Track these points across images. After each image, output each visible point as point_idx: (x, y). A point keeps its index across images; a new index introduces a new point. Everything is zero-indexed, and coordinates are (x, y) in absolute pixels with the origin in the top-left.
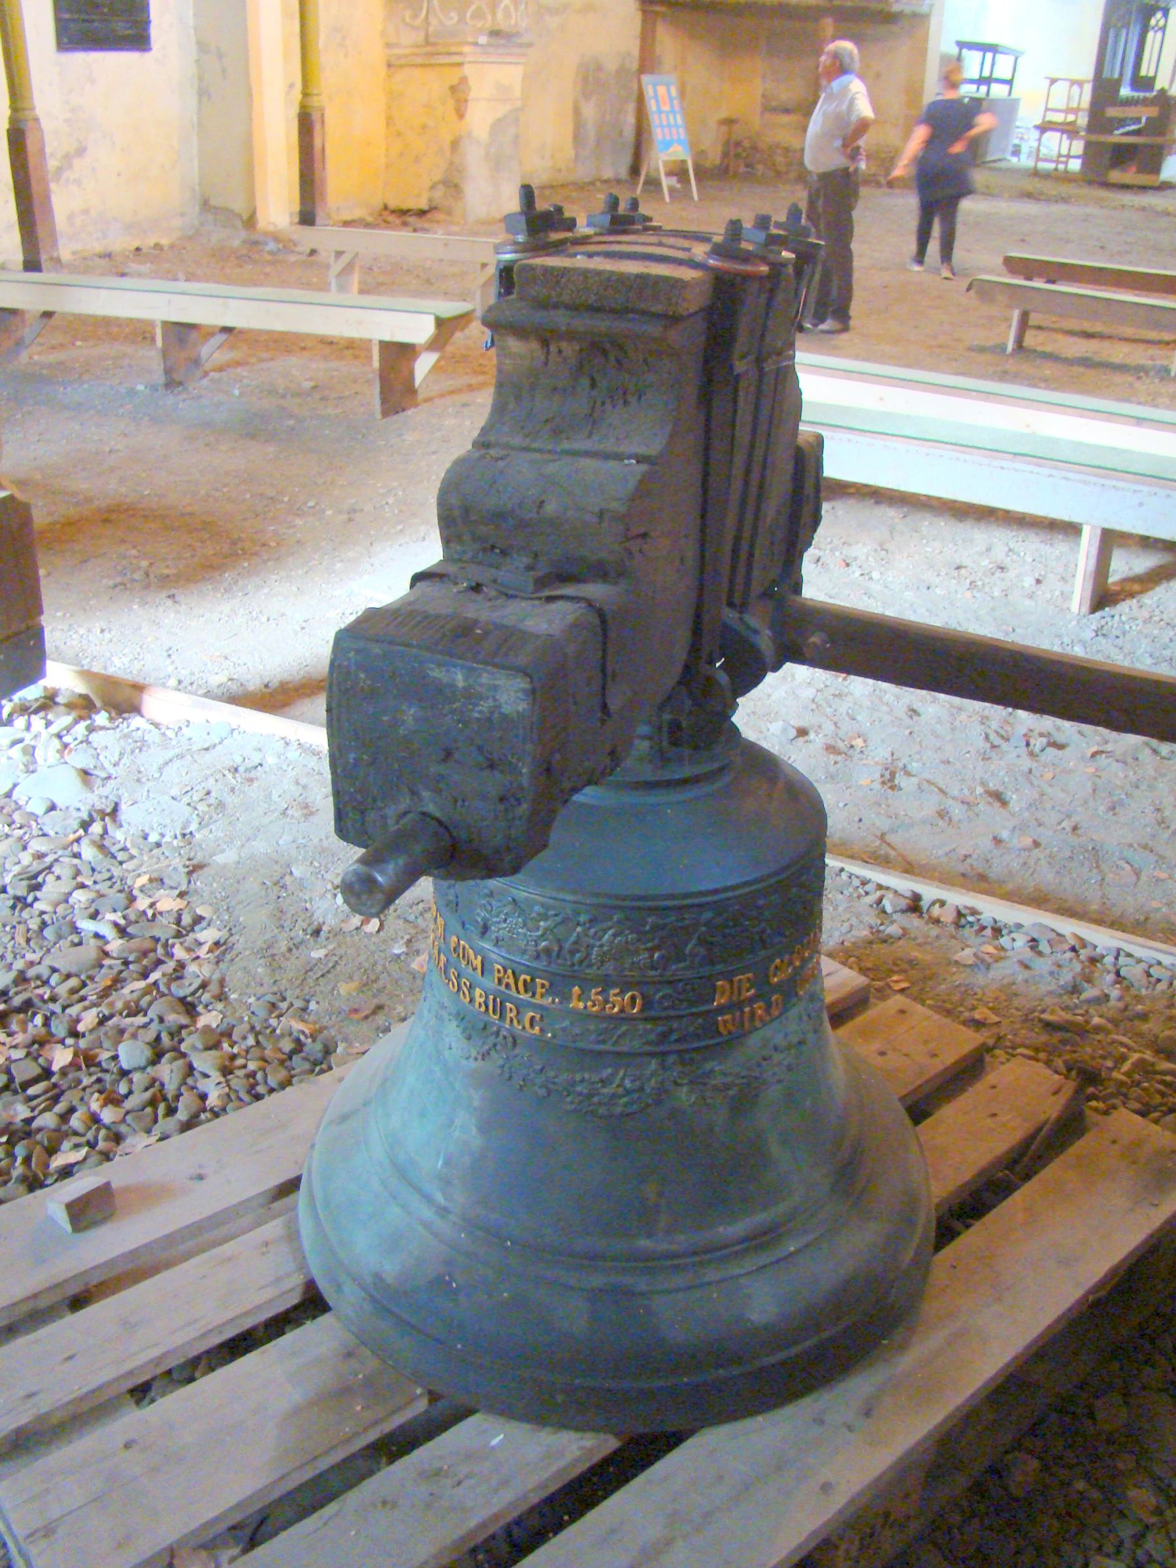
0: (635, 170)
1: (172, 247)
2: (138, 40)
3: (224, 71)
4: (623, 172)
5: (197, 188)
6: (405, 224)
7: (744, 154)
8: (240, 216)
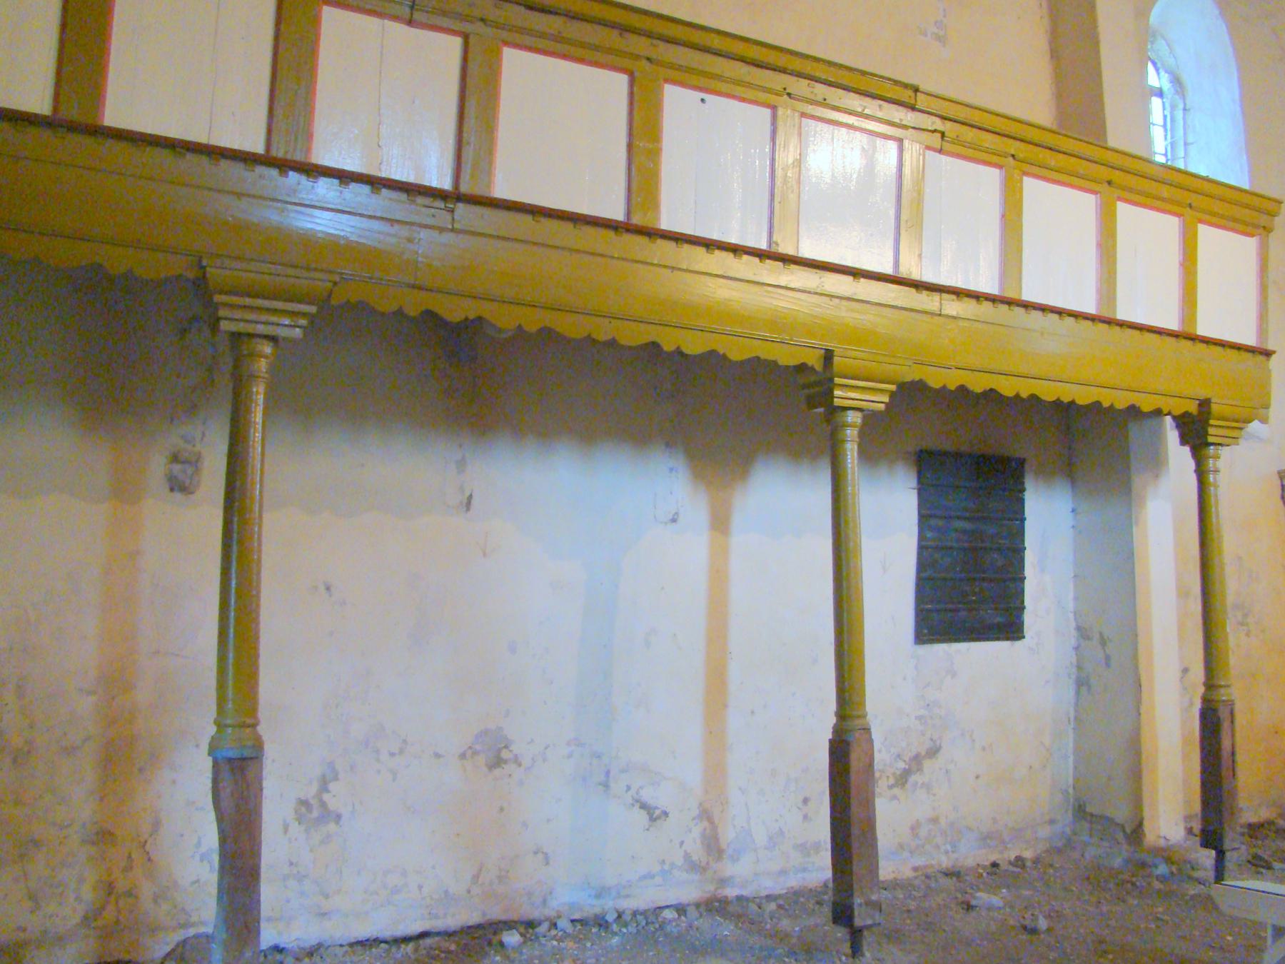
1: (1036, 861)
2: (1011, 628)
3: (1108, 658)
5: (1071, 790)
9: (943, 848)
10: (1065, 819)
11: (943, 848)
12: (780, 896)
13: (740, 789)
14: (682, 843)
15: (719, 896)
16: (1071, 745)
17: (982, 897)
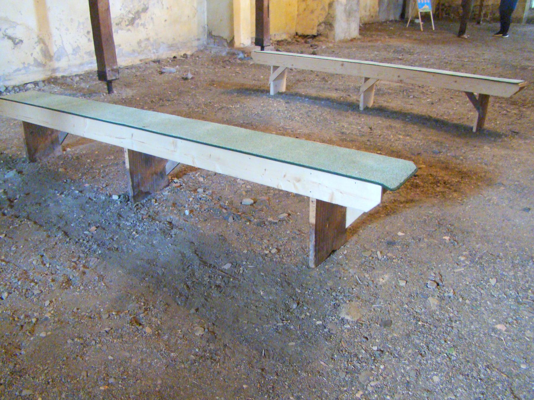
0: (403, 16)
4: (398, 17)
5: (206, 26)
6: (306, 42)
7: (445, 9)
8: (226, 40)
9: (152, 52)
10: (204, 38)
11: (152, 52)
12: (81, 75)
13: (56, 28)
14: (32, 54)
15: (53, 77)
16: (206, 7)
17: (168, 69)
